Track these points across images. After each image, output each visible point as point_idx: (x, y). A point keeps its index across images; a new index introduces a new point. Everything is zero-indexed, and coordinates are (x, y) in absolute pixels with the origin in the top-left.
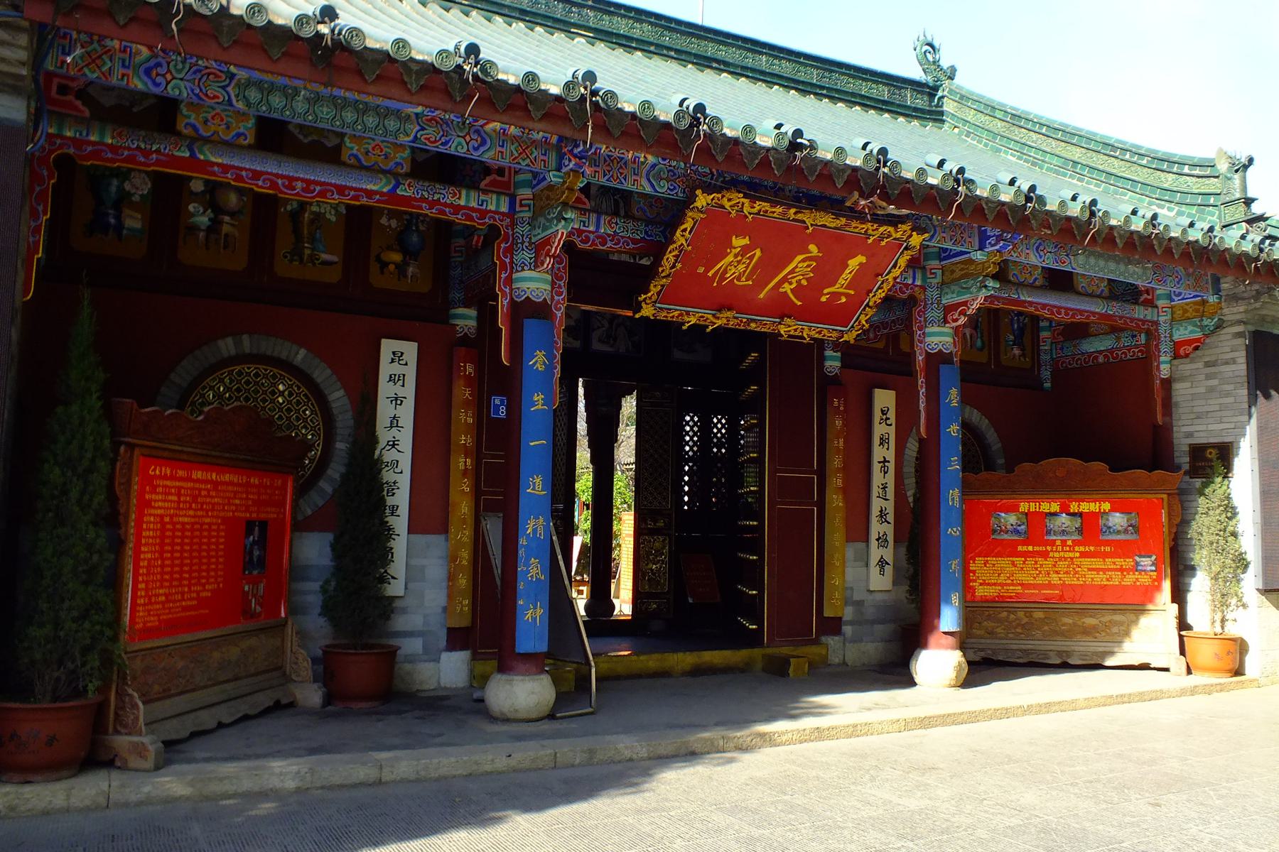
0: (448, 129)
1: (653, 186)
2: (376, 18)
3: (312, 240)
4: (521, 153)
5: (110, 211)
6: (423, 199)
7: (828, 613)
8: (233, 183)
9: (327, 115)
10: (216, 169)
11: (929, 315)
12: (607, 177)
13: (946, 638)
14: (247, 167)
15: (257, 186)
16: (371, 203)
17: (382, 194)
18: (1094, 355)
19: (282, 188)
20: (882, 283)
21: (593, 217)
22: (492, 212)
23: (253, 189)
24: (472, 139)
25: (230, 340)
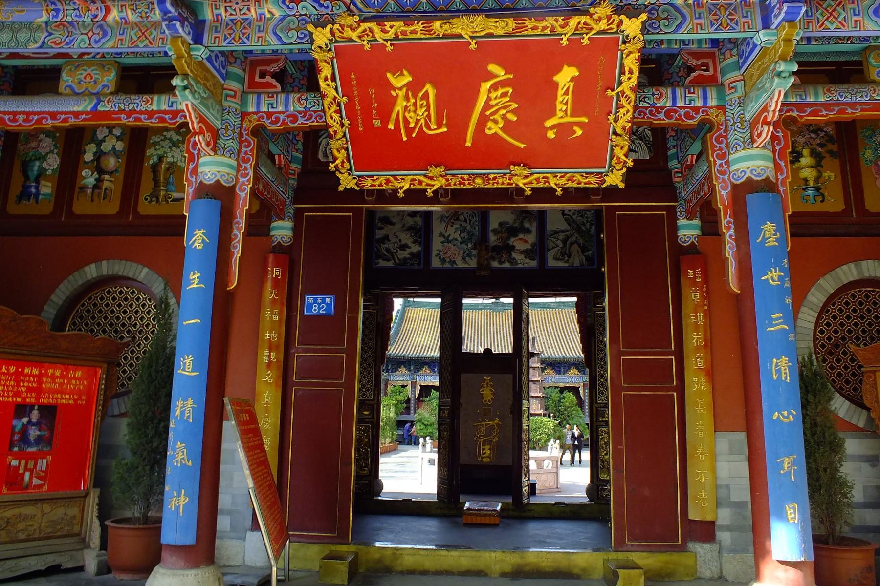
0: (73, 30)
1: (280, 38)
4: (140, 37)
5: (32, 184)
7: (693, 515)
11: (732, 138)
13: (786, 571)
16: (78, 122)
17: (87, 113)
20: (618, 100)
21: (282, 97)
24: (94, 34)
25: (93, 266)
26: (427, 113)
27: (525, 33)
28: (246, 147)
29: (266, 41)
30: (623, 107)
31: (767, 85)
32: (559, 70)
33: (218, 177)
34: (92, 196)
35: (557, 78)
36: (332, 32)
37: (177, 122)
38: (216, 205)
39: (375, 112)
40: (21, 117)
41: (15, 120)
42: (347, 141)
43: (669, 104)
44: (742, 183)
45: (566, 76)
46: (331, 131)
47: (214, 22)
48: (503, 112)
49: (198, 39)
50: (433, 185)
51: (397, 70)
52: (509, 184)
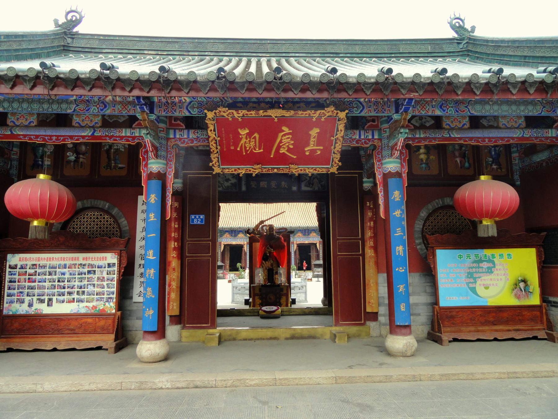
0: (89, 104)
1: (190, 112)
2: (345, 65)
3: (115, 160)
4: (126, 108)
6: (106, 136)
8: (28, 141)
9: (36, 107)
10: (21, 137)
12: (165, 112)
14: (33, 134)
15: (472, 143)
17: (89, 136)
18: (540, 163)
19: (47, 140)
20: (336, 140)
21: (186, 131)
22: (138, 136)
23: (36, 142)
24: (100, 106)
26: (254, 144)
27: (298, 116)
28: (170, 154)
29: (183, 113)
30: (338, 143)
31: (397, 136)
32: (312, 129)
33: (159, 169)
34: (74, 166)
35: (311, 133)
36: (215, 113)
37: (135, 142)
39: (231, 143)
40: (54, 138)
42: (219, 155)
43: (357, 137)
44: (387, 173)
45: (314, 132)
46: (212, 150)
47: (158, 102)
48: (287, 144)
49: (152, 112)
50: (256, 172)
51: (243, 127)
52: (289, 171)
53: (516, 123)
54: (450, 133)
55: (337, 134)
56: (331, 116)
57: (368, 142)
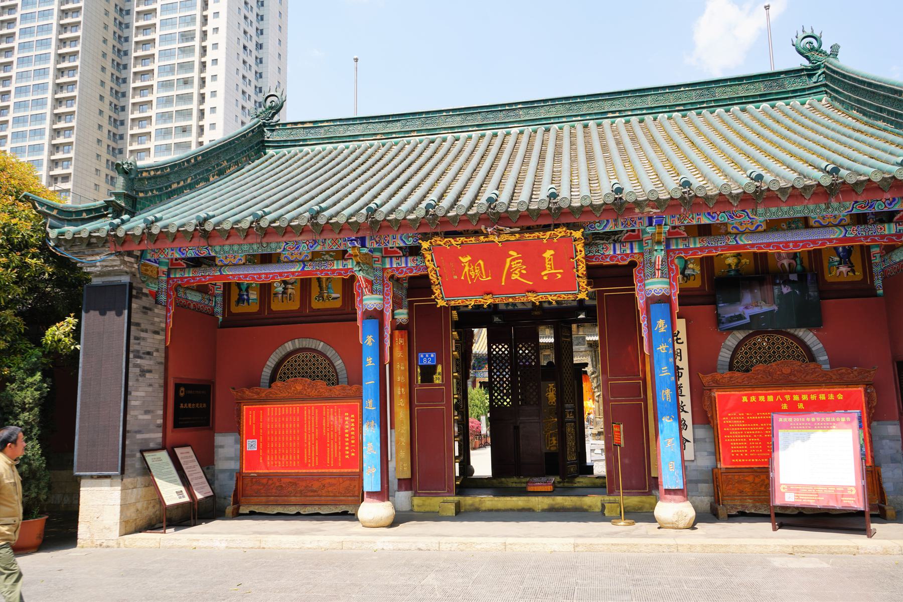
1: (404, 242)
7: (653, 475)
17: (298, 272)
20: (577, 262)
21: (403, 259)
32: (545, 252)
36: (431, 243)
38: (375, 322)
41: (260, 278)
43: (612, 253)
49: (363, 245)
51: (464, 255)
53: (835, 218)
54: (737, 239)
55: (576, 256)
56: (564, 236)
57: (625, 258)
